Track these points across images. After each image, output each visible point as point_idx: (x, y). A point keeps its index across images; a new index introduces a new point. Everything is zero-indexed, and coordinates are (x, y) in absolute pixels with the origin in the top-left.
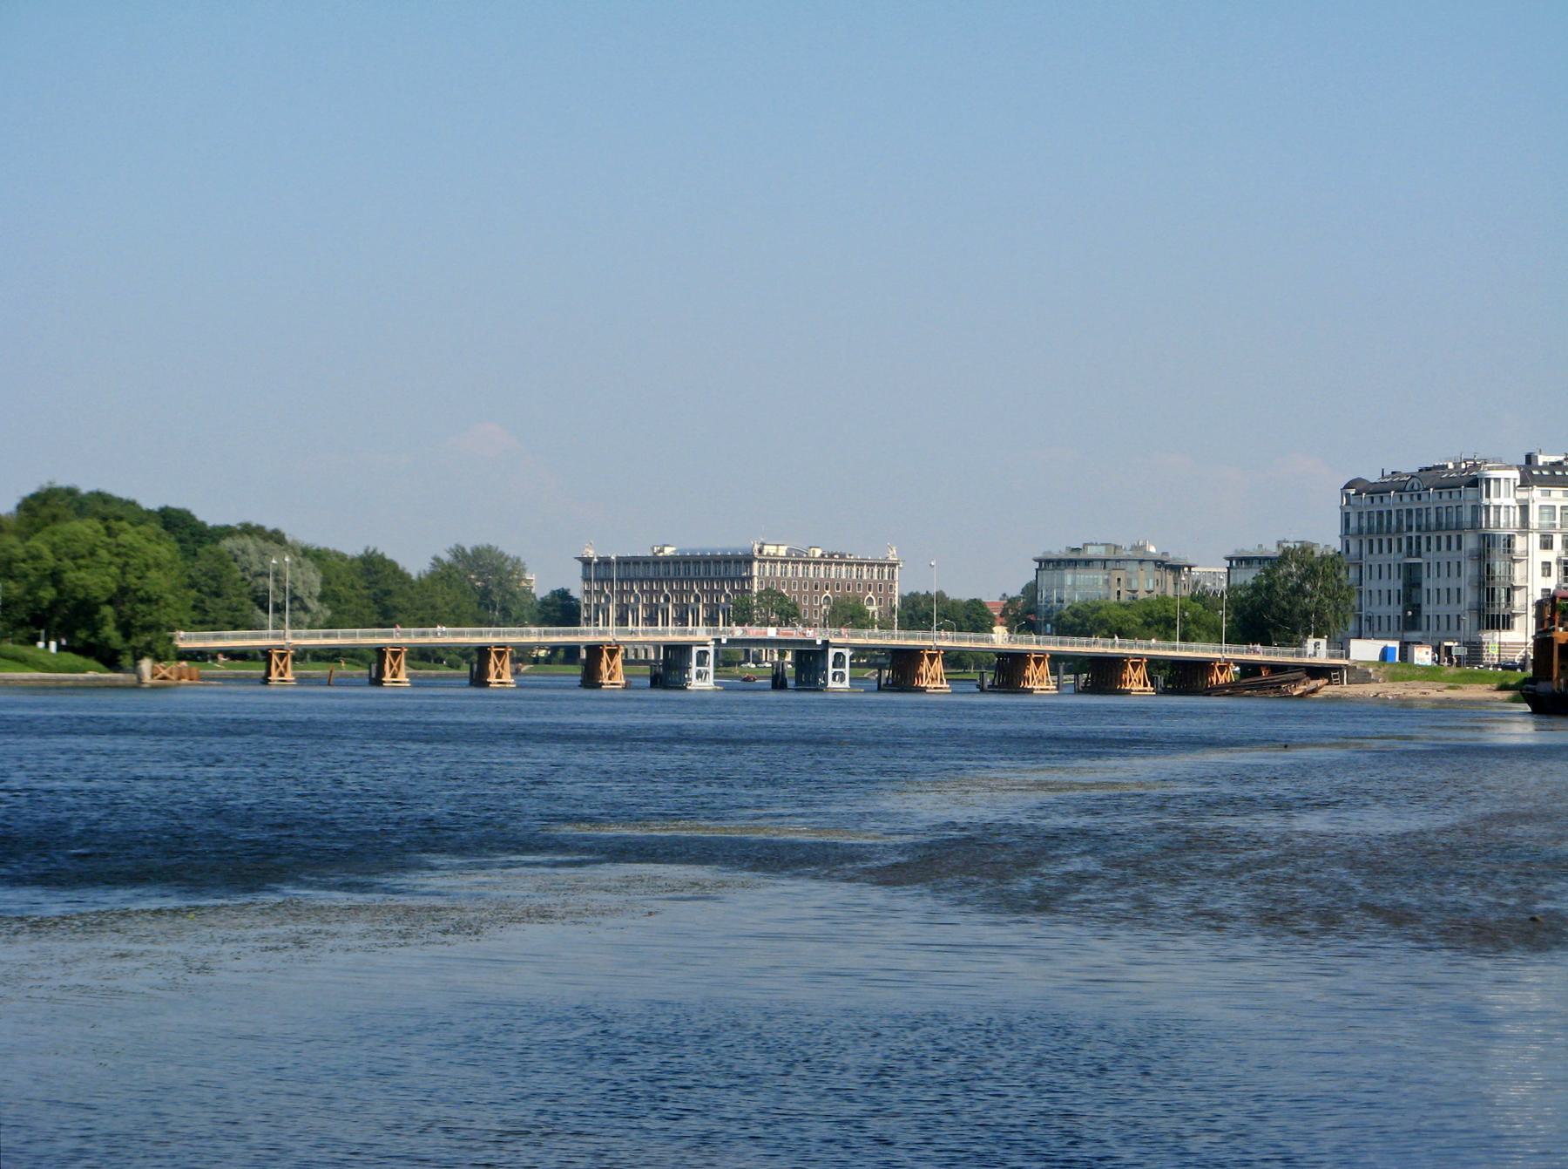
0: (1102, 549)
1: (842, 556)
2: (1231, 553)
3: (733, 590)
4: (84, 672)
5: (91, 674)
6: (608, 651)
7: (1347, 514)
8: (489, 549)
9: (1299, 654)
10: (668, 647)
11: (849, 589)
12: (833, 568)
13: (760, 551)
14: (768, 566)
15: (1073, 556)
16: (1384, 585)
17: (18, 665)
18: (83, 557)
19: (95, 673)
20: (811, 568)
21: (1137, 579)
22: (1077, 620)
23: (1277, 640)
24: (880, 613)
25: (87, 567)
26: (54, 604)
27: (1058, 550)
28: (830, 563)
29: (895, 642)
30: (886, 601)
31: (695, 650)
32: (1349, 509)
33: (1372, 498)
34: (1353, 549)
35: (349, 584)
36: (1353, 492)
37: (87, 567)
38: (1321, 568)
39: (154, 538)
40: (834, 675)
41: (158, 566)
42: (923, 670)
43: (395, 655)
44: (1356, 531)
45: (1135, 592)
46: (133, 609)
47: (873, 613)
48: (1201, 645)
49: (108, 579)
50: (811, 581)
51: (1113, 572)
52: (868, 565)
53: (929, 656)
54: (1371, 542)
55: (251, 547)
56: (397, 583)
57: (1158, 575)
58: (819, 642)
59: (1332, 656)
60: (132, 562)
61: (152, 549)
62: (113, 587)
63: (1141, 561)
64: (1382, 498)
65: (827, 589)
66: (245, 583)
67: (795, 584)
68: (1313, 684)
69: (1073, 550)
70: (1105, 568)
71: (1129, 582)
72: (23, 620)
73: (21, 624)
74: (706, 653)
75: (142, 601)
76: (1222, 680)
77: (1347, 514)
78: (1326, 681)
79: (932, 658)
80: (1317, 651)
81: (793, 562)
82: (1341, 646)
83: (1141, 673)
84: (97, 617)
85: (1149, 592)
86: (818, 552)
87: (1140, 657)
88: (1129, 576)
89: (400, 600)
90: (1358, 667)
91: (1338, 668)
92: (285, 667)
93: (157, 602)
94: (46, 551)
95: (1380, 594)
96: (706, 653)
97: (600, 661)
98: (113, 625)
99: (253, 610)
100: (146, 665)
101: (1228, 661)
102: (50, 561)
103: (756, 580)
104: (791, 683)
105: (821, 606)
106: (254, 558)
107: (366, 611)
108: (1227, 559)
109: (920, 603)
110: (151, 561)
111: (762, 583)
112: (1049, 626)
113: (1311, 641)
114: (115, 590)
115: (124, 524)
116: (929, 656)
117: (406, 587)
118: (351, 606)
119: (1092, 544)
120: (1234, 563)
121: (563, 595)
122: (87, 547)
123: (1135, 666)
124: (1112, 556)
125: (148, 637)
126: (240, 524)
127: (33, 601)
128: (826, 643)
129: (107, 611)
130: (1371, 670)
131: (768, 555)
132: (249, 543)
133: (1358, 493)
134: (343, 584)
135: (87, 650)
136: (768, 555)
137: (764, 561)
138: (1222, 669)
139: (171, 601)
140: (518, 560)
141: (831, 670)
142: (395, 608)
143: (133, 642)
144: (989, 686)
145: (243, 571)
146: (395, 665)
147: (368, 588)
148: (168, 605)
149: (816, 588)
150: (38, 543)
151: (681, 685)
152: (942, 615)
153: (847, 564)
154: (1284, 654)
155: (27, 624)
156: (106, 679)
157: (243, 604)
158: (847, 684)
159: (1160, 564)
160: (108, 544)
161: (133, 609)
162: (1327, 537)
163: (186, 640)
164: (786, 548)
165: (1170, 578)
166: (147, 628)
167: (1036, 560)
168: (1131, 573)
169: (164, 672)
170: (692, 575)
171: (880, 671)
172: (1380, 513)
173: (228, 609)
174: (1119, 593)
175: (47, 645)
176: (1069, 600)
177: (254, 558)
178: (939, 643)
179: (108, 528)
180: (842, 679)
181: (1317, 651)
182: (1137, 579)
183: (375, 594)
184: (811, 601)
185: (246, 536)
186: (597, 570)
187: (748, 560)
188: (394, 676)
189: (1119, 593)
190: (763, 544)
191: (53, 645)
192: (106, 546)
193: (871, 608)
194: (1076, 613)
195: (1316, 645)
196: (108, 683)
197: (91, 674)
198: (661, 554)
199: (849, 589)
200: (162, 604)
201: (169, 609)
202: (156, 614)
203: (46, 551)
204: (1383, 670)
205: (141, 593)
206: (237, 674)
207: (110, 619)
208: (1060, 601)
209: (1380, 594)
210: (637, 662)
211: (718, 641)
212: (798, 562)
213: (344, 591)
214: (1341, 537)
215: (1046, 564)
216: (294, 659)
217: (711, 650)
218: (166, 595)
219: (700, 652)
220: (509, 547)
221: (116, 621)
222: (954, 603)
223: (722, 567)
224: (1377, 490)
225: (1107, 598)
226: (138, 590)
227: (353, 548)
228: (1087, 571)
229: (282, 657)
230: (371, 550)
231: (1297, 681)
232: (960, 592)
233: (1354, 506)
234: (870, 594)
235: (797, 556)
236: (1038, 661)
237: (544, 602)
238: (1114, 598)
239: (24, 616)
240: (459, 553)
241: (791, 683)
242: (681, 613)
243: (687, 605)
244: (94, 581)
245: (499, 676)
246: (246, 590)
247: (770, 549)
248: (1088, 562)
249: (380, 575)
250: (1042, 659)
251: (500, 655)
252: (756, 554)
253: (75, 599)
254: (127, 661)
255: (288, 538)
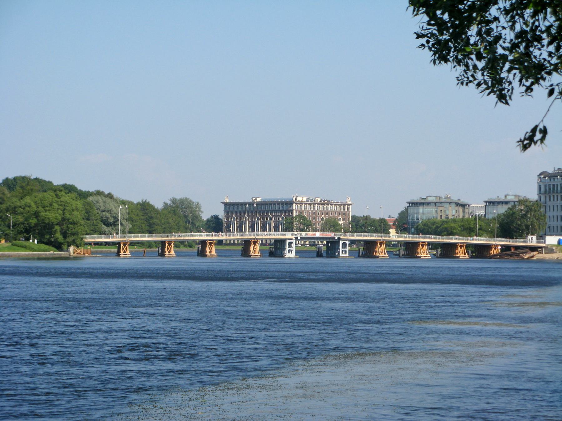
0: (434, 198)
1: (329, 201)
2: (486, 200)
3: (285, 215)
4: (49, 252)
5: (51, 252)
6: (254, 242)
7: (540, 185)
8: (186, 199)
9: (525, 242)
10: (276, 241)
11: (331, 215)
12: (325, 206)
13: (296, 200)
14: (299, 206)
15: (423, 201)
16: (555, 214)
17: (23, 249)
18: (47, 207)
19: (53, 252)
20: (316, 206)
21: (448, 210)
22: (425, 227)
23: (516, 236)
24: (344, 224)
25: (49, 210)
26: (36, 225)
27: (416, 199)
28: (324, 204)
29: (366, 238)
30: (346, 219)
31: (288, 242)
32: (541, 184)
33: (550, 179)
34: (543, 199)
35: (136, 214)
36: (542, 176)
37: (49, 210)
38: (533, 208)
39: (75, 198)
40: (342, 251)
41: (77, 209)
42: (377, 249)
43: (170, 244)
44: (544, 192)
45: (447, 215)
46: (67, 227)
47: (341, 224)
48: (484, 238)
49: (57, 215)
50: (316, 211)
51: (439, 208)
52: (339, 205)
53: (380, 243)
54: (550, 197)
55: (100, 200)
56: (155, 214)
57: (457, 208)
58: (336, 238)
59: (538, 242)
60: (67, 208)
61: (74, 202)
62: (60, 218)
63: (450, 203)
64: (554, 179)
65: (340, 215)
66: (99, 214)
67: (310, 213)
68: (532, 254)
69: (423, 199)
70: (435, 206)
71: (445, 211)
72: (21, 231)
73: (20, 233)
74: (292, 243)
75: (71, 223)
76: (495, 253)
77: (540, 185)
78: (537, 252)
79: (381, 244)
80: (532, 240)
81: (309, 204)
82: (541, 238)
83: (464, 249)
84: (53, 230)
85: (453, 215)
86: (319, 200)
87: (463, 243)
88: (445, 209)
89: (157, 220)
90: (549, 247)
91: (541, 247)
92: (126, 249)
93: (77, 224)
94: (33, 204)
95: (554, 217)
96: (292, 243)
97: (250, 246)
98: (59, 233)
99: (101, 225)
100: (72, 249)
101: (498, 245)
102: (34, 208)
103: (294, 211)
104: (324, 255)
105: (320, 221)
106: (102, 204)
107: (143, 225)
108: (485, 202)
109: (360, 220)
110: (74, 208)
111: (297, 212)
112: (413, 229)
113: (530, 237)
114: (60, 219)
115: (63, 193)
116: (380, 243)
117: (158, 216)
118: (137, 223)
119: (430, 196)
120: (488, 204)
121: (216, 218)
122: (49, 203)
123: (461, 247)
124: (438, 201)
125: (73, 238)
126: (95, 191)
127: (28, 224)
128: (339, 239)
129: (57, 228)
130: (554, 248)
131: (299, 201)
132: (99, 198)
133: (545, 177)
134: (134, 214)
135: (49, 243)
136: (299, 201)
137: (298, 204)
138: (495, 248)
139: (82, 224)
140: (198, 203)
141: (341, 249)
142: (154, 224)
143: (68, 240)
144: (402, 255)
145: (97, 209)
146: (169, 248)
147: (143, 216)
148: (81, 225)
149: (318, 214)
150: (28, 200)
151: (282, 256)
152: (369, 225)
153: (331, 205)
154: (519, 242)
155: (24, 233)
156: (57, 254)
157: (98, 223)
158: (347, 255)
159: (458, 204)
160: (58, 201)
161: (67, 227)
162: (533, 195)
163: (88, 239)
164: (306, 198)
165: (461, 210)
166: (74, 234)
167: (407, 203)
168: (446, 208)
169: (78, 251)
170: (268, 209)
171: (437, 250)
172: (554, 185)
173: (93, 225)
174: (441, 216)
175: (34, 241)
176: (421, 218)
177: (102, 204)
178: (384, 238)
179: (56, 195)
180: (345, 253)
181: (532, 240)
182: (448, 210)
183: (146, 218)
184: (316, 219)
185: (98, 196)
186: (230, 208)
187: (291, 203)
188: (169, 252)
189: (441, 216)
190: (297, 197)
191: (36, 241)
192: (57, 202)
193: (340, 222)
194: (424, 225)
195: (532, 238)
196: (58, 256)
197: (51, 252)
198: (255, 201)
199: (331, 215)
200: (79, 224)
201: (81, 227)
202: (76, 229)
203: (33, 204)
204: (559, 248)
205: (71, 221)
206: (97, 251)
207: (58, 231)
208: (418, 219)
209: (554, 217)
210: (265, 245)
211: (297, 238)
212: (311, 204)
213: (135, 217)
214: (538, 194)
215: (413, 204)
216: (130, 245)
217: (294, 241)
218: (80, 221)
219: (289, 242)
220: (194, 199)
221: (60, 232)
222: (374, 220)
223: (281, 206)
224: (553, 176)
225: (436, 218)
226: (70, 219)
227: (136, 199)
228: (428, 207)
229: (125, 245)
230: (144, 201)
231: (526, 253)
232: (375, 216)
233: (543, 182)
234: (340, 217)
235: (311, 201)
236: (423, 245)
237: (208, 221)
238: (439, 218)
239: (22, 229)
240: (174, 201)
241: (324, 255)
242: (264, 225)
243: (266, 222)
244: (53, 216)
245: (210, 252)
246: (99, 217)
247: (300, 199)
248: (429, 204)
249: (148, 211)
250: (383, 243)
251: (211, 244)
252: (294, 201)
253: (44, 223)
254: (65, 247)
255: (115, 197)
